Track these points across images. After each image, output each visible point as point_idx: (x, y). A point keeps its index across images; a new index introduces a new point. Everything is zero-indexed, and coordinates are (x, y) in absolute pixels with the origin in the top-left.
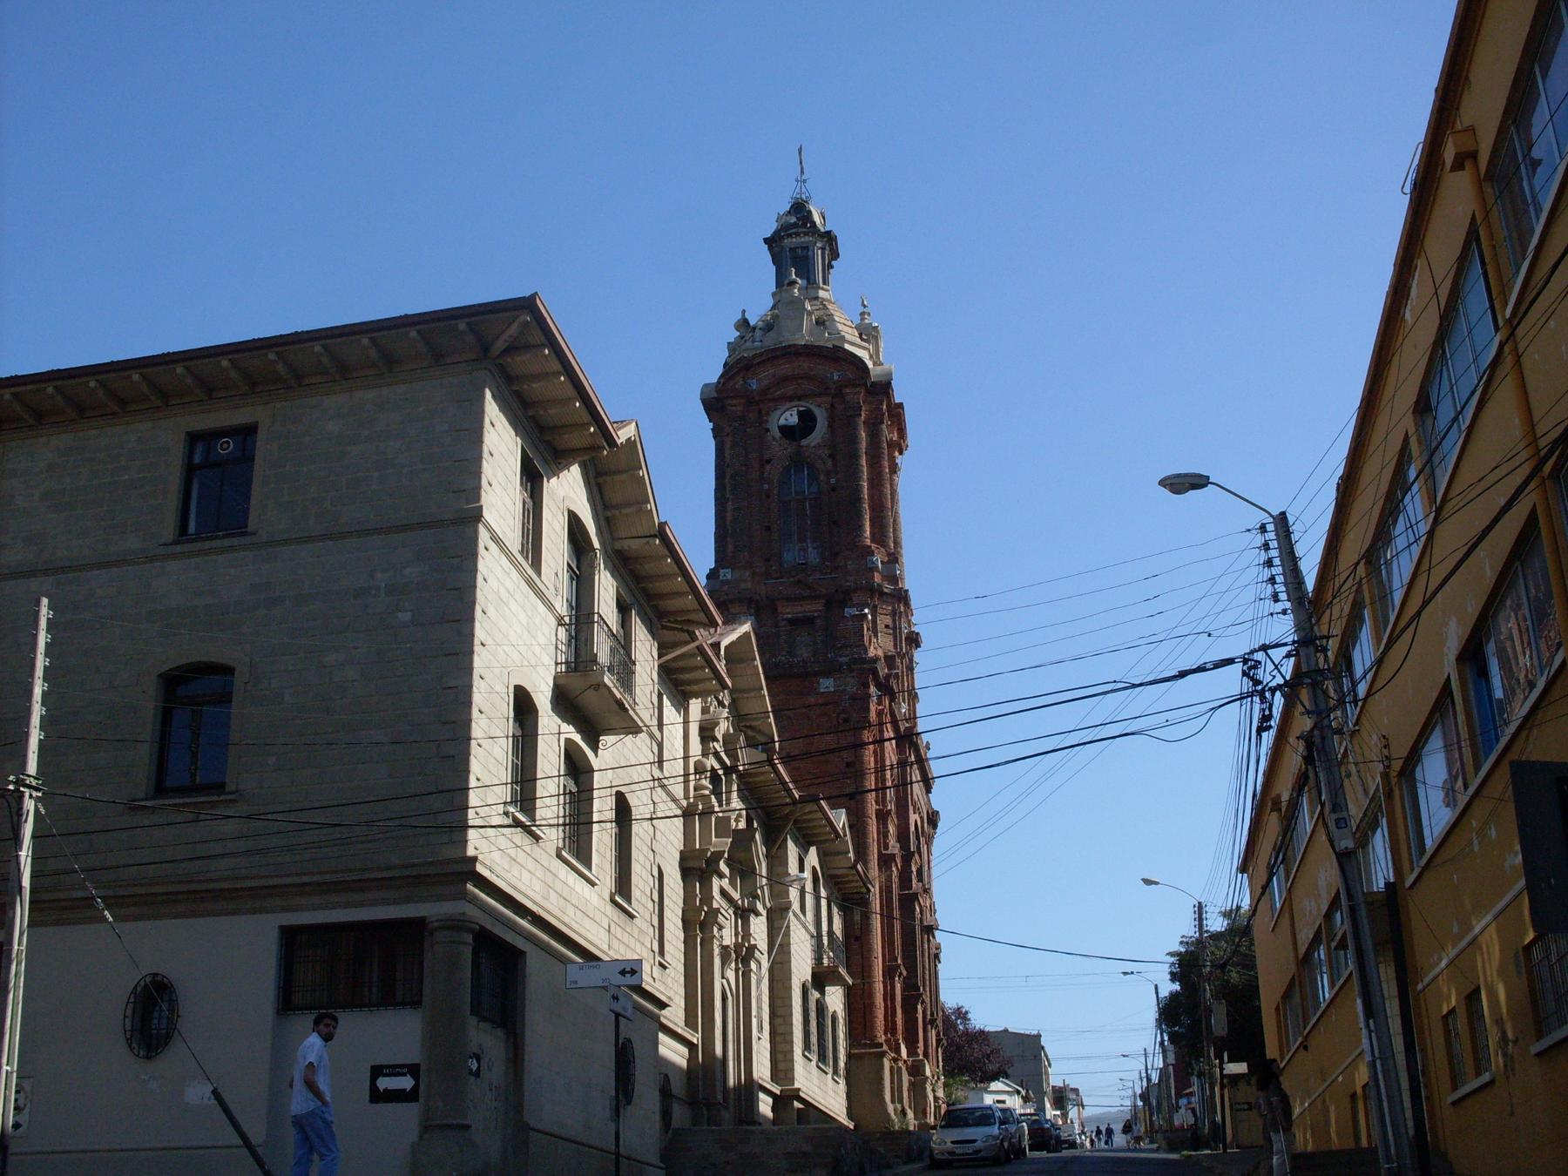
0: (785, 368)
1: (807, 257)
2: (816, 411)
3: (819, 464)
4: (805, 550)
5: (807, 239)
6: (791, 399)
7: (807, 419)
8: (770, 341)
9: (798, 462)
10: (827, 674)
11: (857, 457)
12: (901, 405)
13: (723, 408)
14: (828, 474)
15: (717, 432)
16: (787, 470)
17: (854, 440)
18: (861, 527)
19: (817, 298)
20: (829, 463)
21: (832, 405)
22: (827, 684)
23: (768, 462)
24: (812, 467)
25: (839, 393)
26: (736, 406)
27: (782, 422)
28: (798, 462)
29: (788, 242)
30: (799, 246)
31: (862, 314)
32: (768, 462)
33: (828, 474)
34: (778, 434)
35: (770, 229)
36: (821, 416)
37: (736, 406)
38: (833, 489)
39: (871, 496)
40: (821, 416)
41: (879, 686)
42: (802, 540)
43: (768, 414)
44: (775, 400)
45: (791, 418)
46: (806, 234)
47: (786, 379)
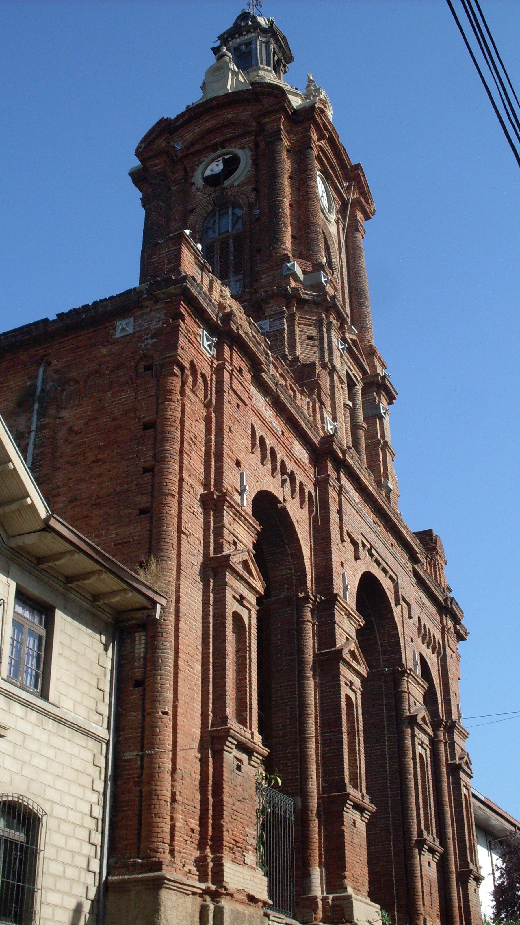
2: (240, 153)
6: (214, 148)
7: (231, 165)
12: (358, 167)
16: (211, 214)
20: (253, 195)
21: (257, 145)
25: (261, 129)
27: (208, 173)
32: (192, 211)
34: (199, 181)
38: (258, 219)
40: (245, 157)
43: (193, 171)
47: (210, 131)
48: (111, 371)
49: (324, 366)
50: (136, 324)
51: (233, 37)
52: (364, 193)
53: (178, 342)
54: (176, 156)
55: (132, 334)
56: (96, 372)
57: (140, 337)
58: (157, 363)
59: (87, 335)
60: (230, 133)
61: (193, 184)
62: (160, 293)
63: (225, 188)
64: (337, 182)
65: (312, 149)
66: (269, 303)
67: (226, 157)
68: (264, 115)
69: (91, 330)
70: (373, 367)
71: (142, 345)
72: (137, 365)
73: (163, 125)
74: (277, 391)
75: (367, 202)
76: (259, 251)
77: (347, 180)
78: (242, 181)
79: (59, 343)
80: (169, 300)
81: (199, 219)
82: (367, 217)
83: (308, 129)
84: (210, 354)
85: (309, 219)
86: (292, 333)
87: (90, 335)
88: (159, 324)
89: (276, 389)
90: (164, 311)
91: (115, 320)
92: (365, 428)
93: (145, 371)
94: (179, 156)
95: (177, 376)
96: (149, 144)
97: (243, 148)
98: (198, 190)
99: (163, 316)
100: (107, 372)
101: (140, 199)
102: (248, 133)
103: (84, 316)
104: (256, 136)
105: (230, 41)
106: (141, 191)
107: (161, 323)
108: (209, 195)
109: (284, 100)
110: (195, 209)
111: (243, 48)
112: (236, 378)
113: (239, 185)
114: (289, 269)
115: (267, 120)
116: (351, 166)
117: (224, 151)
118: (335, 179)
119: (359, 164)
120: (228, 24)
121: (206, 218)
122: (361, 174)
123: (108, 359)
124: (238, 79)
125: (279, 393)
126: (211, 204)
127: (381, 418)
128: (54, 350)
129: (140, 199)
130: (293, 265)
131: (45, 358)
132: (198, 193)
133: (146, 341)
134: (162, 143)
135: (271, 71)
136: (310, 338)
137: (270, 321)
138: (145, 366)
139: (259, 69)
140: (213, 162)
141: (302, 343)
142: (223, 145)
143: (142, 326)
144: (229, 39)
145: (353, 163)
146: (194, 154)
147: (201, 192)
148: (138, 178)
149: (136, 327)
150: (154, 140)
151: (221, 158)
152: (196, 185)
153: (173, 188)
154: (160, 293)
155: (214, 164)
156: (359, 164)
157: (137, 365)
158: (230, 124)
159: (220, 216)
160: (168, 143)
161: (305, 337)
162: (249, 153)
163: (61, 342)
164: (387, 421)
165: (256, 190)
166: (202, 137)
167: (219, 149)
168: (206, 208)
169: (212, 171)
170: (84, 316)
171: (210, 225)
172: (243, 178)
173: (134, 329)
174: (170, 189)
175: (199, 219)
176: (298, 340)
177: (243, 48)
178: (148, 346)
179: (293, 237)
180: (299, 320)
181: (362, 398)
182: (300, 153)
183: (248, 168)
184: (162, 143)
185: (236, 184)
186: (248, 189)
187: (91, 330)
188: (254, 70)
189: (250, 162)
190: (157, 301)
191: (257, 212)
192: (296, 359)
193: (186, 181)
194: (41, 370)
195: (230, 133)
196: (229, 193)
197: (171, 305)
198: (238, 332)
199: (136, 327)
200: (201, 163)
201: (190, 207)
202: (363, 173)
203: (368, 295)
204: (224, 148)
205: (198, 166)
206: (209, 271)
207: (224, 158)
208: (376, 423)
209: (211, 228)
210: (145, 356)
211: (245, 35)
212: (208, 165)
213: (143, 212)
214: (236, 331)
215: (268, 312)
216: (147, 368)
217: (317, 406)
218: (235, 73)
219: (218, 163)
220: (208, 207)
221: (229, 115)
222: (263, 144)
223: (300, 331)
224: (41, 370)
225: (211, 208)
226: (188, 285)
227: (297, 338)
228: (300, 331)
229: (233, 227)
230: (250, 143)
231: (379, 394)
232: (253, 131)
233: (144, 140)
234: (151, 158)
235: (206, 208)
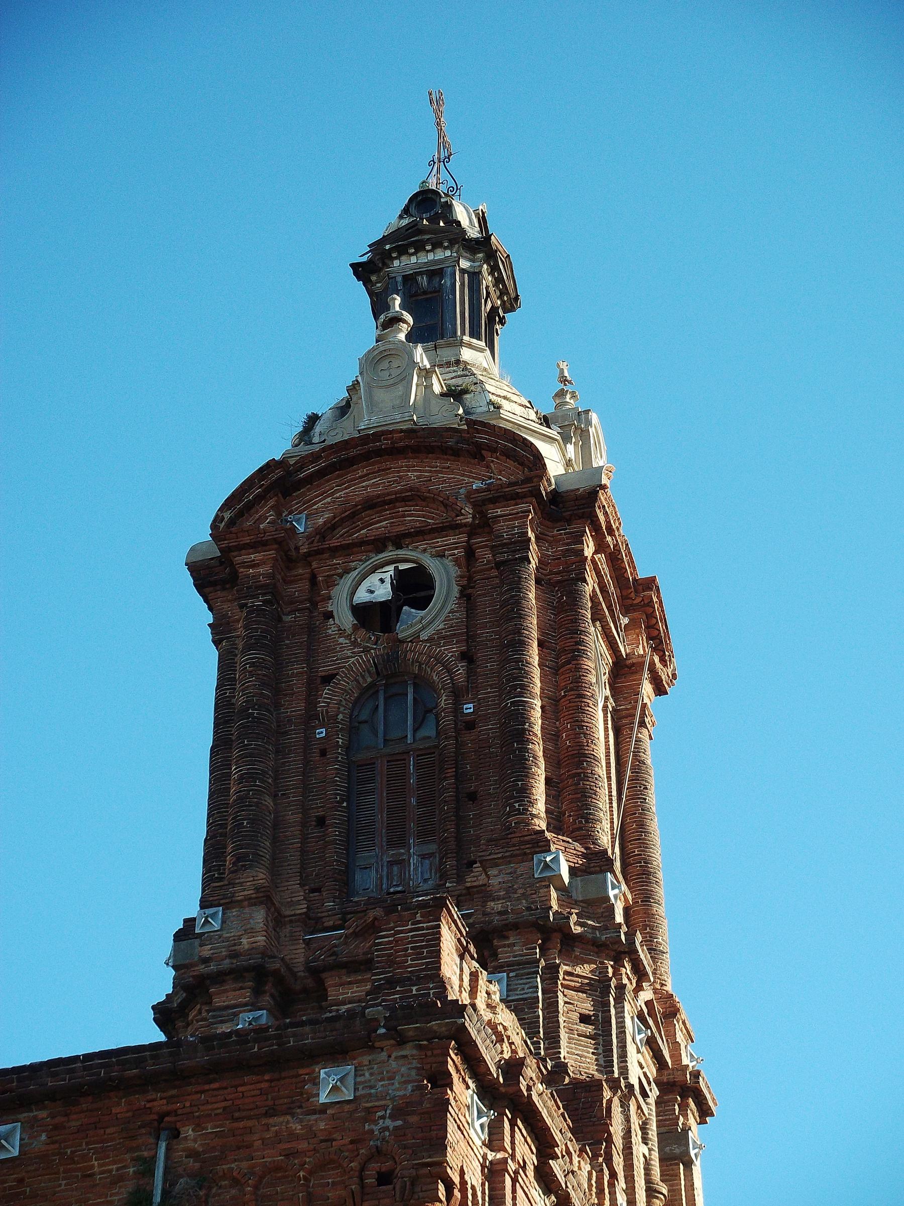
0: (368, 484)
1: (439, 290)
2: (433, 566)
3: (437, 676)
4: (402, 863)
5: (440, 254)
6: (379, 544)
7: (413, 588)
8: (346, 431)
9: (393, 676)
10: (336, 1053)
11: (520, 645)
12: (650, 583)
13: (233, 579)
14: (458, 695)
15: (220, 632)
16: (368, 693)
17: (513, 611)
18: (524, 793)
19: (458, 362)
20: (461, 670)
21: (470, 553)
22: (330, 1084)
23: (328, 679)
24: (422, 683)
25: (483, 524)
26: (258, 565)
27: (362, 596)
28: (393, 676)
29: (401, 265)
30: (430, 270)
31: (561, 394)
32: (328, 679)
33: (458, 695)
34: (345, 619)
35: (360, 253)
36: (444, 574)
37: (258, 565)
38: (470, 725)
39: (551, 736)
40: (444, 574)
41: (488, 1092)
42: (398, 840)
43: (330, 583)
44: (347, 550)
45: (378, 587)
46: (437, 245)
47: (372, 504)
48: (311, 1172)
49: (614, 1085)
50: (359, 1079)
51: (402, 251)
52: (659, 644)
53: (446, 1137)
54: (297, 549)
55: (348, 1102)
56: (278, 1168)
57: (369, 1111)
58: (406, 1173)
59: (259, 1086)
60: (414, 517)
61: (329, 615)
62: (408, 1028)
63: (402, 641)
64: (612, 625)
65: (585, 581)
66: (507, 938)
67: (403, 566)
68: (494, 501)
69: (267, 1077)
70: (675, 1047)
71: (375, 1128)
72: (363, 1169)
73: (274, 477)
74: (567, 1187)
75: (663, 661)
76: (473, 797)
77: (626, 612)
78: (438, 632)
79: (197, 1093)
80: (425, 1042)
81: (344, 703)
82: (660, 690)
83: (578, 539)
84: (480, 1138)
85: (581, 746)
86: (552, 1007)
87: (263, 1085)
88: (405, 1089)
89: (566, 1184)
90: (415, 1064)
91: (317, 1063)
92: (664, 1195)
93: (379, 1185)
94: (304, 550)
95: (441, 1201)
96: (240, 514)
97: (441, 555)
98: (341, 632)
99: (413, 1073)
100: (301, 1174)
101: (209, 625)
102: (453, 527)
103: (256, 1050)
104: (471, 535)
105: (396, 258)
106: (210, 609)
107: (410, 1087)
108: (366, 650)
109: (541, 478)
110: (333, 676)
111: (423, 281)
112: (522, 1188)
113: (430, 640)
114: (547, 866)
115: (499, 512)
116: (635, 580)
117: (402, 553)
118: (609, 619)
119: (653, 579)
120: (385, 216)
121: (358, 699)
122: (655, 599)
123: (303, 1145)
124: (429, 387)
125: (570, 1190)
126: (369, 672)
127: (689, 1164)
128: (188, 1104)
129: (209, 625)
130: (556, 860)
131: (166, 1119)
132: (341, 640)
133: (381, 1121)
134: (266, 518)
135: (481, 350)
136: (584, 1019)
137: (508, 977)
138: (378, 1173)
139: (461, 344)
140: (374, 572)
141: (571, 1030)
142: (398, 541)
143: (371, 1087)
144: (394, 255)
145: (642, 574)
146: (334, 551)
147: (348, 637)
148: (208, 576)
149: (361, 1087)
150: (249, 506)
151: (391, 568)
152: (337, 621)
153: (288, 618)
154: (408, 1028)
155: (374, 579)
156: (653, 579)
157: (363, 1169)
158: (414, 496)
159: (386, 699)
160: (279, 514)
161: (575, 1016)
162: (454, 571)
163: (202, 1092)
164: (697, 1170)
165: (467, 657)
166: (353, 515)
167: (390, 548)
168: (361, 680)
169: (372, 592)
170: (256, 1050)
171: (363, 717)
172: (439, 625)
173: (356, 1089)
174: (280, 620)
175: (344, 703)
176: (562, 1025)
177: (423, 281)
178: (387, 1133)
179: (548, 781)
180: (564, 979)
181: (657, 1127)
182: (562, 584)
183: (451, 605)
184: (266, 518)
185: (424, 636)
186: (451, 651)
187: (267, 1077)
188: (449, 345)
189: (456, 591)
190: (402, 1041)
191: (469, 708)
192: (561, 1068)
193: (314, 604)
194: (163, 1146)
195: (414, 517)
196: (410, 656)
197: (429, 1053)
198: (530, 1096)
199: (361, 1087)
200: (347, 571)
201: (323, 670)
202: (659, 597)
203: (660, 875)
204: (399, 547)
205: (341, 576)
206: (472, 958)
207: (396, 568)
208: (678, 1175)
209: (366, 722)
210: (378, 1151)
211: (428, 251)
212: (364, 577)
213: (213, 655)
214: (526, 1094)
215: (505, 956)
216: (384, 1179)
217: (606, 1178)
218: (424, 373)
219: (383, 576)
220: (363, 677)
221: (413, 473)
222: (485, 556)
223: (566, 1003)
224: (163, 1146)
225: (369, 680)
226: (466, 1024)
227: (561, 1019)
228: (566, 1003)
229: (415, 730)
230: (456, 548)
231: (684, 1108)
232: (465, 525)
233: (228, 504)
234: (240, 548)
235: (361, 680)
